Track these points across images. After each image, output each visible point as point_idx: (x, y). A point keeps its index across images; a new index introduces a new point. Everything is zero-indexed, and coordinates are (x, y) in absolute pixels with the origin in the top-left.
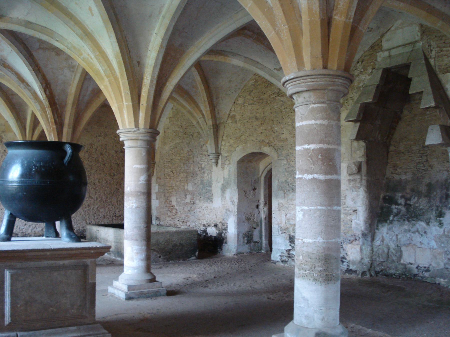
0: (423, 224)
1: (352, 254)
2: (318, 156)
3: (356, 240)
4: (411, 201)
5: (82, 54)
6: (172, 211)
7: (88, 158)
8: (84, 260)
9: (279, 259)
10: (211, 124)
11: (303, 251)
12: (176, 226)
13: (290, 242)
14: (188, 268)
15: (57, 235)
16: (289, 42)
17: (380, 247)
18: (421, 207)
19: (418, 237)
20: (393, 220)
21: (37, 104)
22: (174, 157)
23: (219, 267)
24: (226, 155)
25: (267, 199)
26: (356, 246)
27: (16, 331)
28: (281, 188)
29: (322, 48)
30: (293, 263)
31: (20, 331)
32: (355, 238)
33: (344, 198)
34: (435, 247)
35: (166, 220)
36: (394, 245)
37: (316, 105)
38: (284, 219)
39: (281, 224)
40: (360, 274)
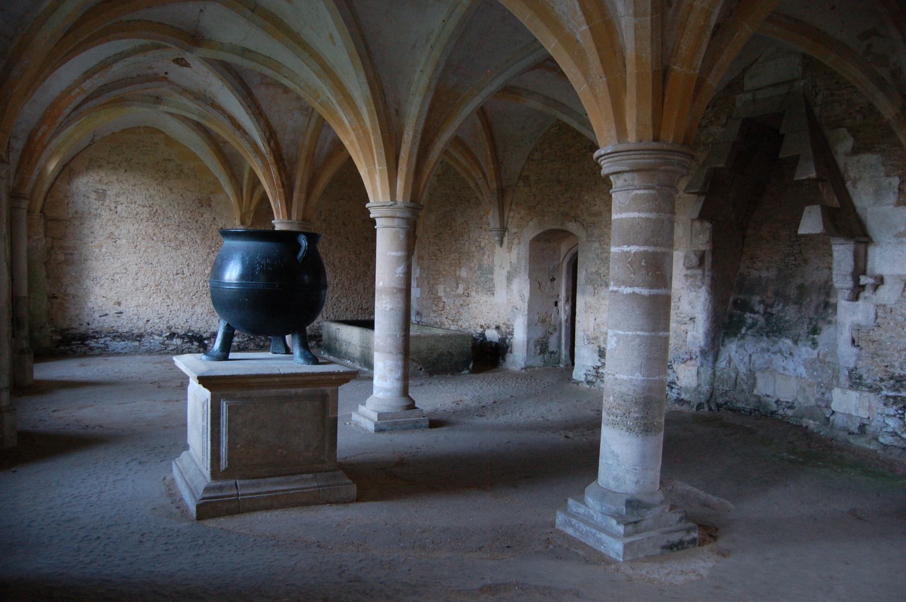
0: (789, 342)
1: (686, 378)
2: (640, 262)
3: (691, 359)
4: (774, 309)
5: (318, 97)
6: (438, 304)
7: (326, 230)
8: (323, 388)
9: (583, 378)
10: (495, 187)
11: (614, 390)
12: (443, 327)
13: (600, 356)
14: (459, 386)
15: (288, 351)
16: (606, 102)
17: (725, 370)
18: (788, 318)
19: (781, 360)
20: (746, 334)
21: (258, 159)
22: (442, 230)
23: (501, 387)
24: (514, 230)
25: (570, 293)
26: (691, 368)
27: (235, 478)
28: (590, 281)
29: (653, 111)
30: (602, 386)
31: (240, 479)
32: (691, 356)
33: (677, 300)
34: (804, 375)
35: (429, 316)
36: (746, 368)
37: (641, 192)
38: (592, 324)
39: (588, 331)
40: (695, 406)
